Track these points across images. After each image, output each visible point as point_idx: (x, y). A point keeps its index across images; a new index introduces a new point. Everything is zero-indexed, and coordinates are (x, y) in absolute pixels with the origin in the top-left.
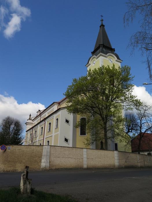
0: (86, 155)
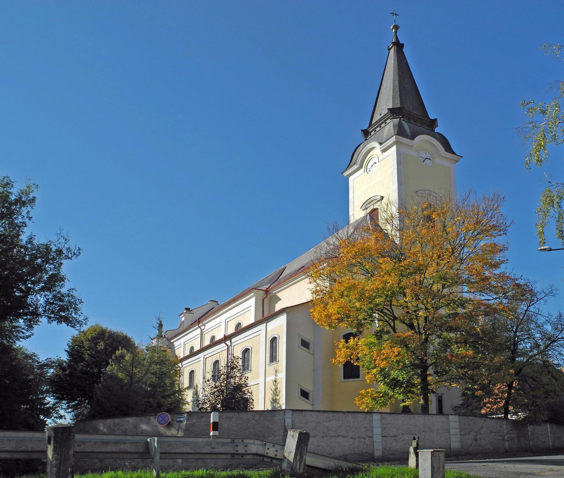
0: (380, 429)
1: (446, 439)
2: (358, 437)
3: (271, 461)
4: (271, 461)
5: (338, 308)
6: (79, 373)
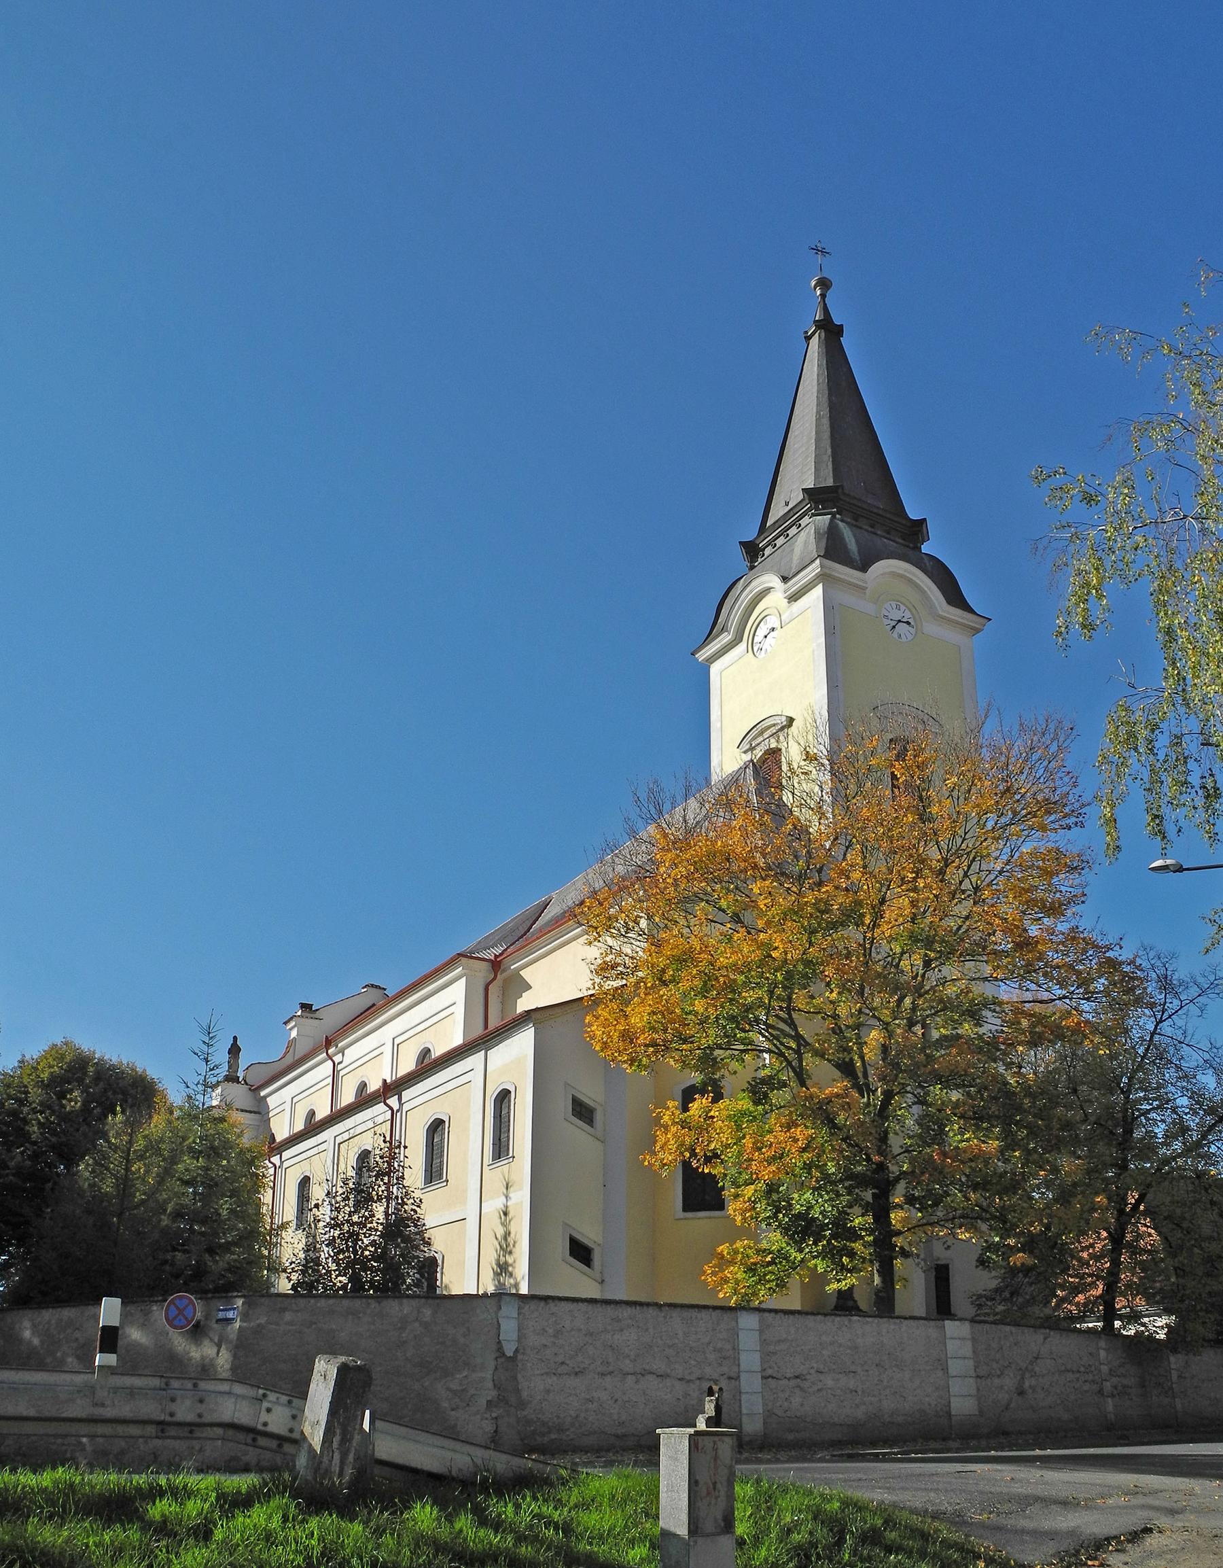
0: (757, 1356)
1: (937, 1388)
2: (699, 1379)
3: (280, 1446)
4: (280, 1446)
5: (649, 1014)
6: (13, 1175)
